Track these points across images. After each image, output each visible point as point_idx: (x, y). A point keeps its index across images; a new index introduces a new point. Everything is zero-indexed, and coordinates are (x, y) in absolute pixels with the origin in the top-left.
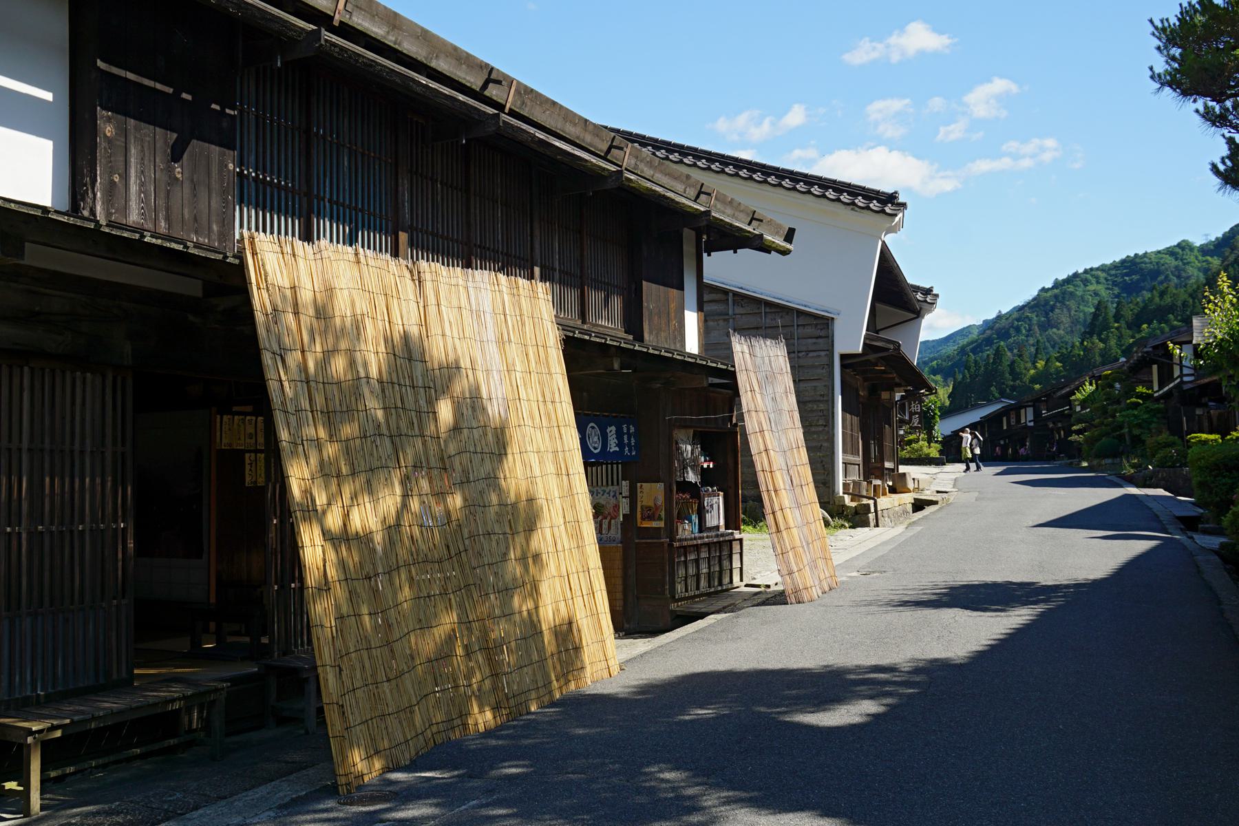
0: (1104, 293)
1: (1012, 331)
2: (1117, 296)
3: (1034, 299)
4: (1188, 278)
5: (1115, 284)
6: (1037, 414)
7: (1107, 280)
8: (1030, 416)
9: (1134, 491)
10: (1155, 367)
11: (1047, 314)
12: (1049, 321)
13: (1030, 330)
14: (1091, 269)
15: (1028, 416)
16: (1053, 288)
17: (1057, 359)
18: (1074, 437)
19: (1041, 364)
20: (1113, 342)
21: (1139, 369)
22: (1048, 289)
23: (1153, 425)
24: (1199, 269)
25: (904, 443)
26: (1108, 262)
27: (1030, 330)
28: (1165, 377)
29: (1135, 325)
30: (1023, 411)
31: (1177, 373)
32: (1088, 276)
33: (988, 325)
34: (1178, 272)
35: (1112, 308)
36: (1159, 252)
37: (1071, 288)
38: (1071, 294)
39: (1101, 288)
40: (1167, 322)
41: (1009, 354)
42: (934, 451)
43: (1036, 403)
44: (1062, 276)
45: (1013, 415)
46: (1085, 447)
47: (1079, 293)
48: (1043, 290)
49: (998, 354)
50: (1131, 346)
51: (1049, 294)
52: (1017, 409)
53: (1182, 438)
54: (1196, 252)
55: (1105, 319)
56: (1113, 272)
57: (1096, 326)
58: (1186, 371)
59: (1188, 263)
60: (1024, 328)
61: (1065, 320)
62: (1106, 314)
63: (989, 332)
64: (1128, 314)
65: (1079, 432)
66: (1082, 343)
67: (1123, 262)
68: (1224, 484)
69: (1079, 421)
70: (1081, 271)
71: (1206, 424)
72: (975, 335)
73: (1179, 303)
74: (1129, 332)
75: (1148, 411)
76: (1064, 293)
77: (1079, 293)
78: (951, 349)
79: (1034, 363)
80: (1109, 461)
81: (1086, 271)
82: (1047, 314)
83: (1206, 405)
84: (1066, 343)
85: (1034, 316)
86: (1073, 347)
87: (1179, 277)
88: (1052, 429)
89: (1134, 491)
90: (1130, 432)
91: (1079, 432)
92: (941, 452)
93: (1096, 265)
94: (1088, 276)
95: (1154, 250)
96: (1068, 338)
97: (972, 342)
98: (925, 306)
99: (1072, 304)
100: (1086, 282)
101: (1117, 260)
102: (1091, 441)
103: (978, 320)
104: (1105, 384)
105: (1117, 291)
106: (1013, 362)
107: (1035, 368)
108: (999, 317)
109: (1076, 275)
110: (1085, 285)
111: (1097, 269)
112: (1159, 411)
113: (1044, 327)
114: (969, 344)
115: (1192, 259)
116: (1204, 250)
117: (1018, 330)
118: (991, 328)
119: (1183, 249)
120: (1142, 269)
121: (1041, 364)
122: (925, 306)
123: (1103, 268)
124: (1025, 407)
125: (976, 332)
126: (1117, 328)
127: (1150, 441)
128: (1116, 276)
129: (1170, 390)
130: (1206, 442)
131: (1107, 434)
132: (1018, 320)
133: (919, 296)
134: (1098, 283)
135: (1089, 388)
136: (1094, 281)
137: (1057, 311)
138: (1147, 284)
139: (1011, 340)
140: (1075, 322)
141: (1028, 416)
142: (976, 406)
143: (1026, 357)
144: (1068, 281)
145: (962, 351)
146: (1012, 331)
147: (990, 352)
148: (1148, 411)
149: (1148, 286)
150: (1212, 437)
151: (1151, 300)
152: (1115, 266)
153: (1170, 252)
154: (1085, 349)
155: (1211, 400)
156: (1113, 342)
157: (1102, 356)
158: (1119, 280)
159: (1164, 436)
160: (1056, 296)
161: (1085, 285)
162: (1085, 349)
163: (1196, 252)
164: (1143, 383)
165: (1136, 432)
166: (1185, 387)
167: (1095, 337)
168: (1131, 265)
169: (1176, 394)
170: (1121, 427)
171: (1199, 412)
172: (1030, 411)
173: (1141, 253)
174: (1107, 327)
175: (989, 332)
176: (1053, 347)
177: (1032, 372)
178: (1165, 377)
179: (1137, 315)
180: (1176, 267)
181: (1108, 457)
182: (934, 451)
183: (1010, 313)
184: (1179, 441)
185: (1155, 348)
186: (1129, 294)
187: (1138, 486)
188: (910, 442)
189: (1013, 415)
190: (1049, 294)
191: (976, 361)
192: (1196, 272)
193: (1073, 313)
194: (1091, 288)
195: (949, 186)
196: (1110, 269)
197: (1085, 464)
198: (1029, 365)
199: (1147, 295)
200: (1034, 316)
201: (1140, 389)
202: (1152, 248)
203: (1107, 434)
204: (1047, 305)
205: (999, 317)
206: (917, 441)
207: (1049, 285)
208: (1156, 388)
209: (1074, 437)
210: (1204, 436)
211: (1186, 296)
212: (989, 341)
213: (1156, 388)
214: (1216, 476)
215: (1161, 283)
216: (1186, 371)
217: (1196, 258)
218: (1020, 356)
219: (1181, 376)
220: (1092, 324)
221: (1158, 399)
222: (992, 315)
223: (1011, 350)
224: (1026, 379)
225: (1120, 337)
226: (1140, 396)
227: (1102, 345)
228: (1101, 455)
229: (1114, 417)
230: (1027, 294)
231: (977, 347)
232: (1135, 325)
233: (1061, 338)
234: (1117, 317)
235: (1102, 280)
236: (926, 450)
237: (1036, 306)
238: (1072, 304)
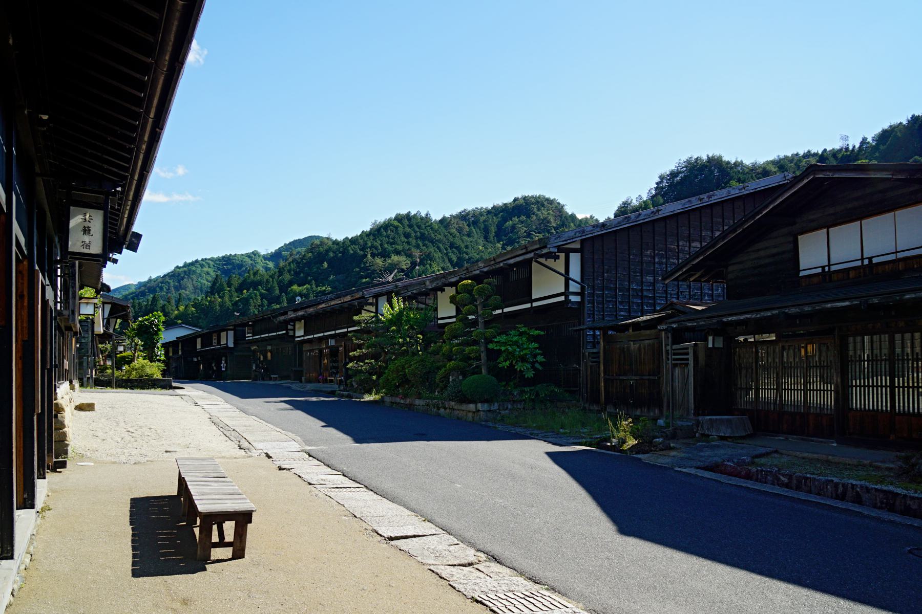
1: (158, 289)
15: (228, 339)
17: (193, 306)
19: (182, 308)
20: (227, 299)
25: (120, 363)
26: (215, 256)
29: (239, 290)
37: (194, 268)
40: (257, 290)
42: (155, 370)
44: (189, 261)
47: (198, 272)
48: (177, 267)
50: (237, 302)
60: (165, 287)
65: (360, 359)
67: (223, 257)
72: (133, 289)
74: (236, 294)
76: (190, 270)
81: (203, 260)
82: (179, 282)
91: (360, 359)
92: (164, 373)
93: (208, 257)
97: (132, 293)
99: (194, 277)
100: (202, 266)
103: (135, 282)
105: (361, 241)
106: (164, 306)
108: (150, 280)
109: (197, 261)
113: (177, 288)
116: (266, 258)
117: (161, 289)
121: (182, 308)
123: (212, 259)
124: (227, 330)
132: (162, 283)
143: (173, 301)
144: (192, 264)
152: (219, 259)
153: (248, 255)
156: (227, 299)
157: (220, 306)
160: (185, 272)
175: (143, 288)
177: (176, 312)
182: (155, 370)
191: (139, 304)
194: (206, 269)
198: (174, 308)
202: (239, 252)
207: (181, 265)
212: (143, 294)
218: (169, 302)
220: (212, 287)
222: (144, 279)
224: (173, 316)
225: (231, 296)
227: (220, 300)
230: (170, 268)
232: (239, 290)
237: (173, 276)
238: (194, 277)
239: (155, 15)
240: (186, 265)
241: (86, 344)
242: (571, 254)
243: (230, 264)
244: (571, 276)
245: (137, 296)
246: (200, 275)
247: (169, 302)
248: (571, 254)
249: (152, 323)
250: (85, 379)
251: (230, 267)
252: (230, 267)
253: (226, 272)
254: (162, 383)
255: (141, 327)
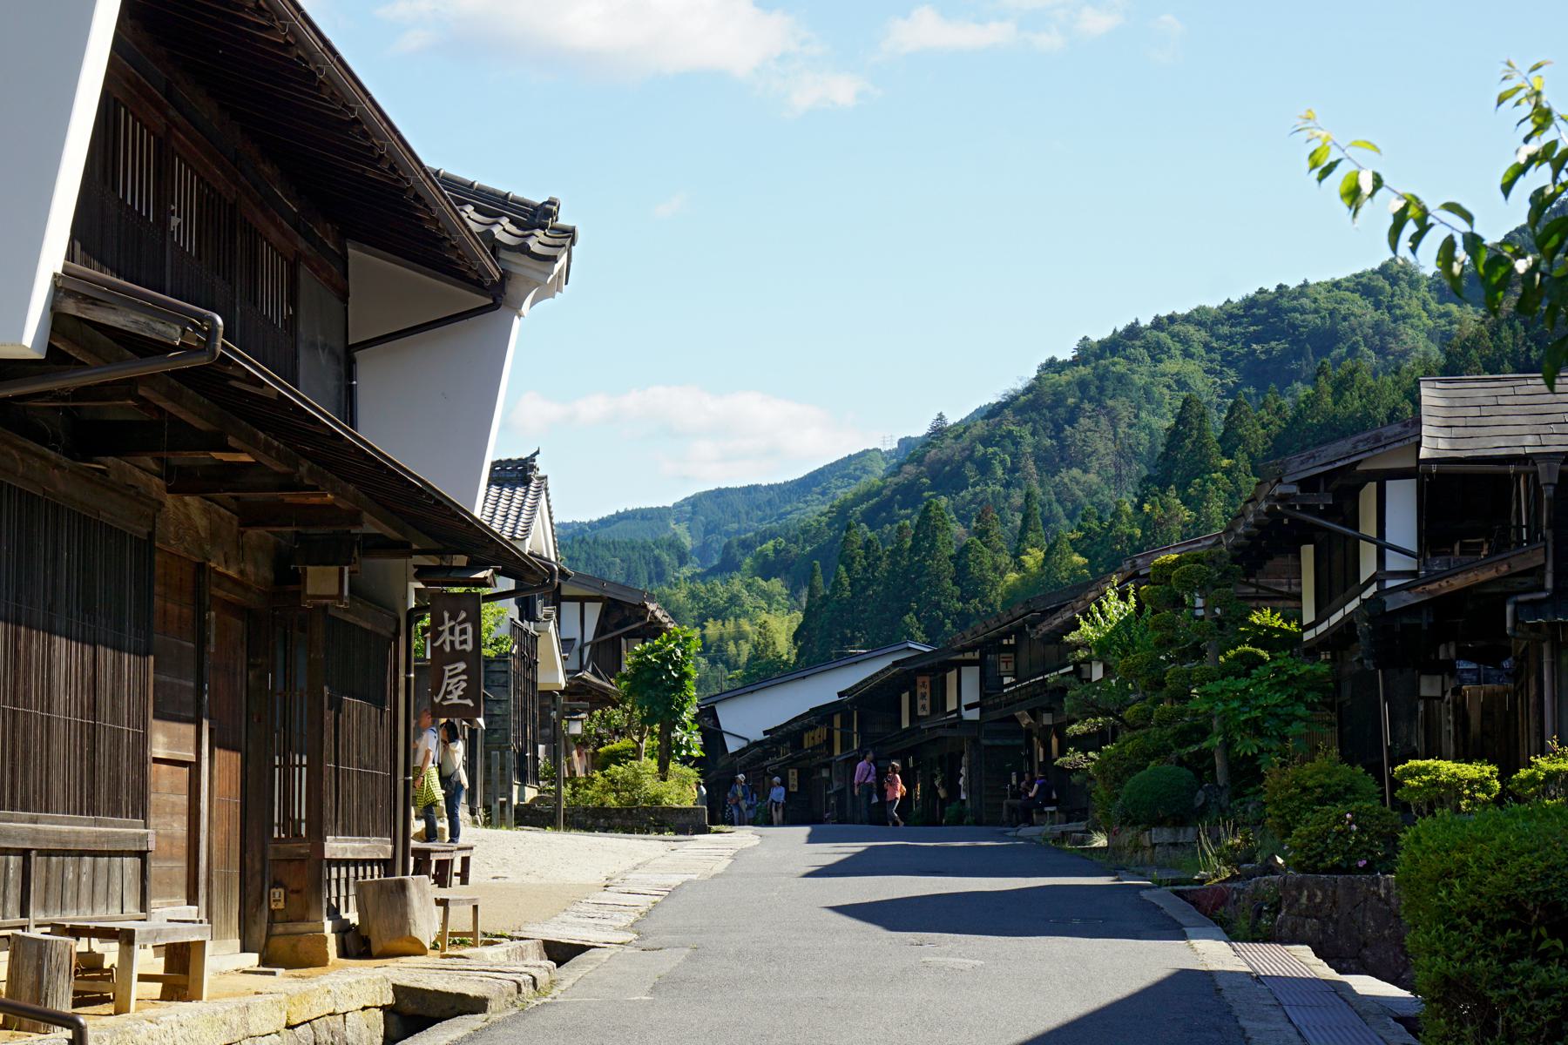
0: (1202, 385)
1: (970, 471)
2: (1231, 392)
3: (1028, 390)
4: (1404, 354)
5: (1229, 360)
6: (989, 685)
7: (1208, 348)
8: (971, 694)
9: (1213, 954)
10: (1308, 552)
11: (1059, 429)
12: (1063, 447)
13: (1014, 469)
14: (1172, 319)
15: (966, 689)
16: (1074, 363)
18: (1073, 758)
19: (1033, 558)
21: (1262, 548)
22: (1065, 365)
23: (1297, 728)
24: (1430, 335)
26: (1214, 302)
27: (1014, 469)
28: (1337, 578)
30: (952, 676)
31: (1368, 568)
32: (1163, 336)
33: (912, 452)
34: (1381, 339)
35: (1216, 423)
36: (1336, 285)
37: (1121, 366)
38: (1120, 378)
39: (1193, 370)
41: (957, 529)
43: (987, 652)
45: (924, 687)
46: (1100, 789)
47: (1139, 380)
48: (1051, 365)
49: (928, 528)
51: (1067, 376)
52: (937, 669)
53: (1376, 771)
54: (1423, 290)
55: (1200, 444)
56: (1225, 330)
57: (1175, 464)
58: (1394, 562)
59: (1405, 317)
61: (1103, 446)
62: (1202, 432)
63: (910, 469)
64: (1256, 435)
65: (1084, 743)
66: (1139, 507)
67: (1250, 304)
68: (1544, 992)
69: (1089, 709)
70: (1146, 321)
71: (1448, 727)
72: (875, 476)
73: (1382, 413)
75: (1285, 682)
77: (1139, 380)
78: (813, 511)
79: (1016, 556)
80: (1164, 835)
81: (1158, 324)
83: (1447, 668)
84: (1102, 507)
85: (1026, 431)
86: (1116, 515)
87: (1381, 351)
88: (1029, 733)
89: (1213, 954)
90: (1228, 745)
93: (1182, 310)
94: (1163, 336)
95: (1326, 277)
96: (1107, 495)
97: (868, 495)
98: (519, 265)
99: (1121, 406)
100: (1157, 352)
101: (1236, 299)
102: (1117, 773)
104: (1162, 593)
105: (1232, 377)
106: (965, 550)
107: (1020, 566)
109: (1133, 331)
110: (1156, 360)
111: (1187, 319)
112: (1315, 683)
113: (1050, 463)
114: (860, 499)
115: (1414, 307)
117: (984, 466)
118: (918, 460)
119: (1394, 280)
120: (1294, 327)
121: (1033, 558)
122: (519, 265)
123: (1198, 318)
125: (880, 469)
126: (1228, 472)
127: (1276, 777)
128: (1230, 339)
129: (1348, 623)
130: (1454, 787)
131: (1161, 752)
132: (986, 441)
133: (504, 231)
134: (1187, 354)
135: (1116, 608)
136: (1176, 349)
137: (1084, 422)
138: (1307, 366)
139: (966, 495)
140: (1126, 454)
141: (966, 689)
142: (857, 661)
144: (1116, 345)
145: (841, 515)
146: (970, 471)
147: (909, 520)
148: (1285, 682)
149: (1309, 371)
150: (1471, 771)
151: (1312, 401)
154: (1147, 523)
155: (1463, 654)
158: (1238, 349)
159: (1327, 766)
160: (1082, 384)
161: (1156, 360)
162: (1147, 523)
163: (1423, 290)
164: (1271, 598)
165: (1246, 746)
166: (1391, 604)
167: (1172, 491)
168: (1267, 315)
169: (1363, 626)
170: (1204, 732)
171: (1429, 687)
172: (971, 677)
173: (1293, 283)
174: (1201, 467)
175: (910, 469)
176: (1071, 516)
177: (1012, 577)
178: (1337, 578)
179: (1277, 439)
180: (1377, 326)
181: (1160, 823)
183: (965, 426)
184: (1369, 784)
185: (1308, 485)
186: (1262, 388)
187: (1232, 934)
188: (616, 757)
189: (924, 687)
190: (1067, 376)
192: (1422, 343)
193: (1122, 429)
194: (1170, 366)
195: (843, 90)
196: (1217, 321)
197: (1100, 841)
198: (1005, 559)
199: (1302, 390)
200: (1026, 431)
201: (1263, 617)
202: (1319, 275)
203: (1161, 752)
204: (1058, 404)
205: (939, 431)
206: (636, 754)
207: (1066, 354)
208: (1309, 616)
209: (1073, 758)
210: (1447, 767)
211: (1397, 396)
212: (909, 494)
213: (1309, 616)
214: (1513, 954)
215: (1337, 363)
216: (1394, 562)
217: (1425, 304)
218: (982, 534)
219: (1379, 577)
221: (1312, 651)
223: (964, 519)
226: (1265, 638)
227: (1186, 514)
228: (1141, 815)
229: (1185, 697)
230: (1011, 375)
231: (879, 506)
233: (1091, 493)
234: (1229, 443)
235: (1198, 349)
236: (651, 785)
239: (163, 678)
240: (1088, 353)
241: (505, 717)
242: (1388, 483)
243: (1276, 334)
244: (1389, 539)
245: (886, 505)
246: (1147, 391)
247: (982, 534)
248: (1388, 483)
249: (667, 658)
250: (496, 807)
251: (1277, 346)
252: (1277, 346)
253: (1263, 374)
254: (681, 820)
255: (641, 666)
